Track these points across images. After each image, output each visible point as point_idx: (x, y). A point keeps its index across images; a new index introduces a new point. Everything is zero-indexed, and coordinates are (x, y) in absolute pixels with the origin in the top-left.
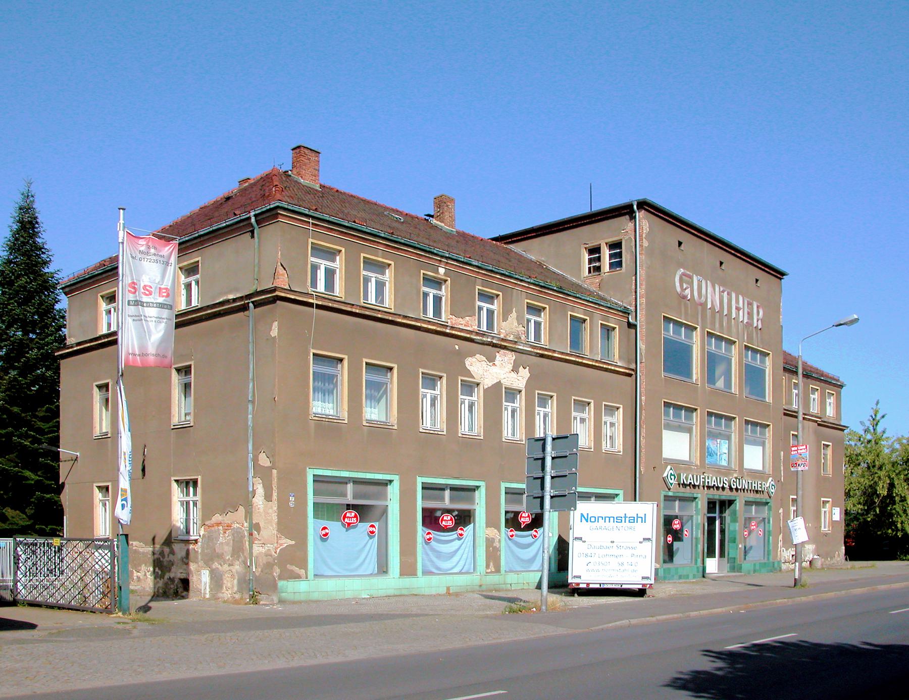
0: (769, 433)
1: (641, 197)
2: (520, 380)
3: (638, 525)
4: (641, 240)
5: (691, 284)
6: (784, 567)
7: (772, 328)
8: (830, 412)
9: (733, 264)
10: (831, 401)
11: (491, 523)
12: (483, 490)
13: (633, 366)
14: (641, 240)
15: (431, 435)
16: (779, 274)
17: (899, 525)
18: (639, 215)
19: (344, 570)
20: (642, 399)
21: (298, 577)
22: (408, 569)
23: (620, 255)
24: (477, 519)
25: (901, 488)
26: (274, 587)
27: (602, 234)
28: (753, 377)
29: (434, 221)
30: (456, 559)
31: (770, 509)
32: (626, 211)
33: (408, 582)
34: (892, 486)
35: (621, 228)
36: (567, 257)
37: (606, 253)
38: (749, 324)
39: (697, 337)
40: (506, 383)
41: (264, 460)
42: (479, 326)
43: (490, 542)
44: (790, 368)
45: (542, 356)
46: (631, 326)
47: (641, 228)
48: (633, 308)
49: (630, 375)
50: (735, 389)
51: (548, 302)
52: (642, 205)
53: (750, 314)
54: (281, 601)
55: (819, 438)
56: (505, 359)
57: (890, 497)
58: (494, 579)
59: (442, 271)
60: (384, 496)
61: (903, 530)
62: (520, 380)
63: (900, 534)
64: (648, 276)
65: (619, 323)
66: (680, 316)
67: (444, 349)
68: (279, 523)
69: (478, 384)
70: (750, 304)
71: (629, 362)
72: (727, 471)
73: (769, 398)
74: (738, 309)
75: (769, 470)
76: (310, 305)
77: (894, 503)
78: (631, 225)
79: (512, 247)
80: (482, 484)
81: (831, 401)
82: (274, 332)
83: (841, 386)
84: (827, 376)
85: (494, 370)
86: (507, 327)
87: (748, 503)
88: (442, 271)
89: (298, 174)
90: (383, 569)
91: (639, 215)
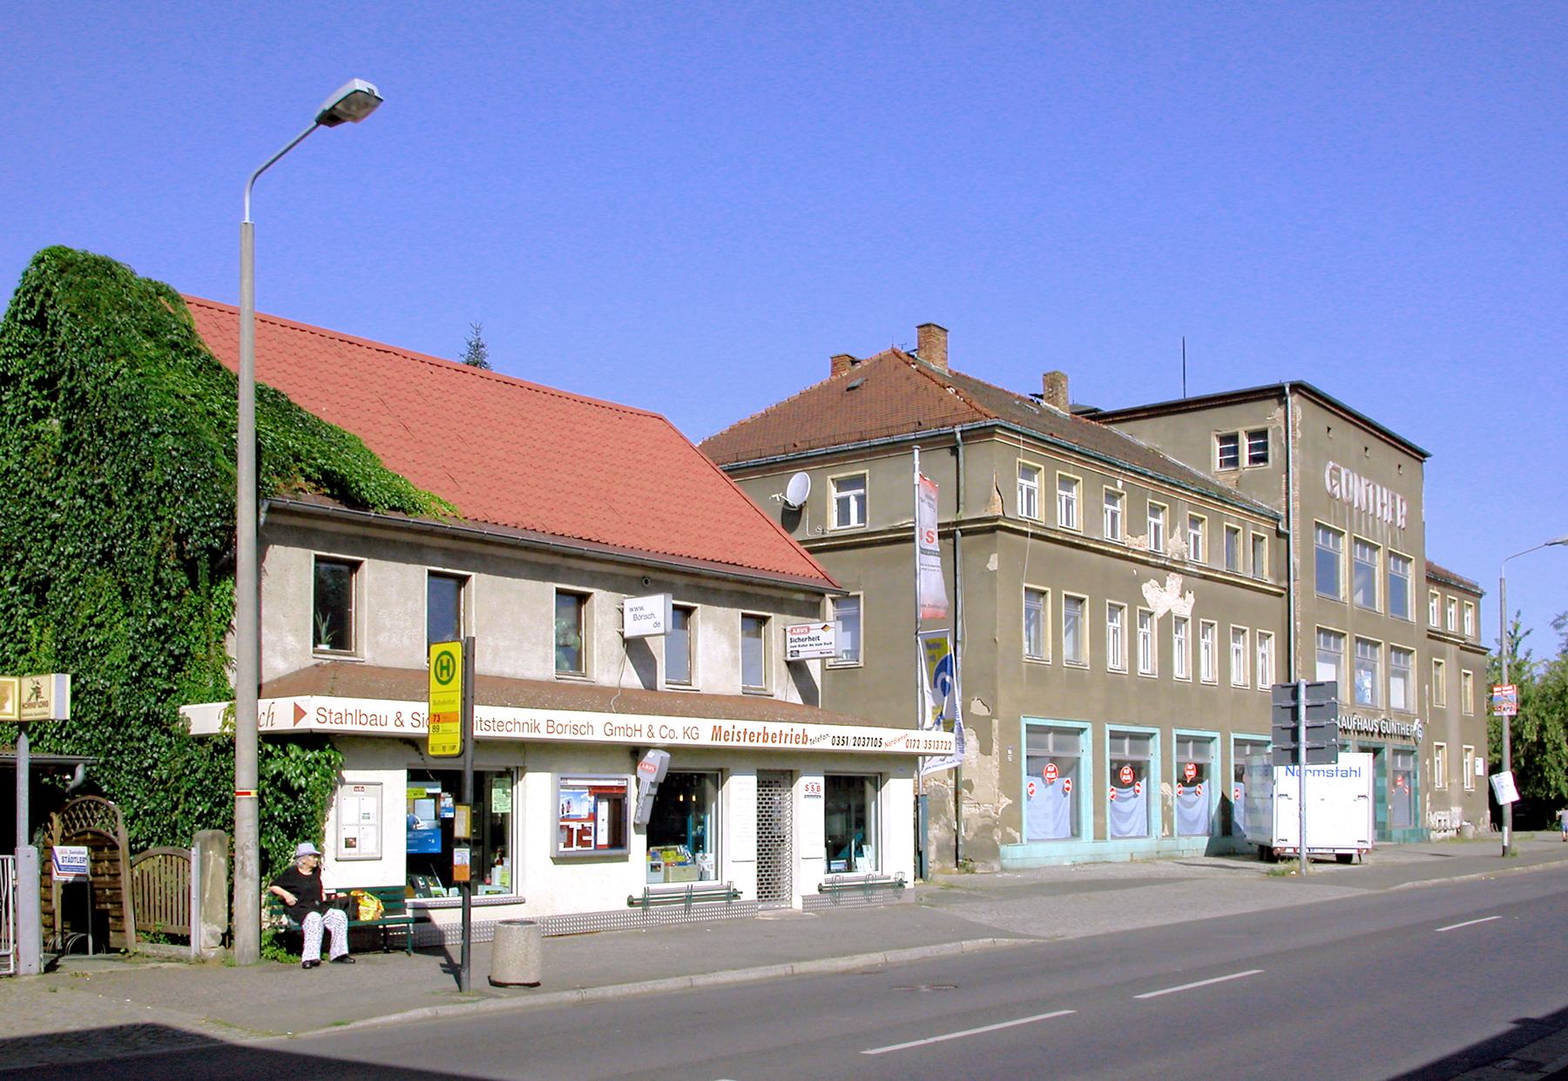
0: (1413, 661)
1: (1296, 379)
2: (1184, 607)
3: (1352, 779)
4: (1294, 430)
5: (1339, 479)
6: (1433, 835)
7: (1415, 530)
8: (1469, 630)
9: (1379, 448)
10: (1469, 614)
11: (1166, 778)
12: (1158, 737)
13: (1284, 584)
14: (1294, 430)
15: (1181, 682)
16: (1420, 455)
17: (1553, 783)
18: (1292, 400)
19: (1047, 836)
20: (1297, 625)
21: (1014, 841)
22: (1100, 835)
23: (1265, 446)
24: (1152, 773)
25: (1555, 732)
26: (994, 852)
27: (1241, 421)
28: (1396, 586)
29: (1044, 403)
30: (1132, 819)
31: (1416, 760)
32: (1275, 393)
33: (1100, 845)
34: (1542, 728)
35: (1270, 415)
36: (1196, 447)
37: (1245, 443)
38: (1393, 523)
39: (1344, 543)
40: (1175, 612)
41: (978, 708)
42: (1157, 546)
43: (1164, 799)
44: (1437, 578)
45: (1205, 577)
46: (1279, 533)
47: (1294, 416)
48: (1283, 513)
49: (1280, 595)
50: (1379, 606)
51: (1206, 511)
52: (1297, 387)
53: (1394, 511)
54: (1003, 869)
55: (1462, 664)
56: (1174, 581)
57: (1541, 744)
58: (1168, 843)
59: (1120, 484)
60: (1076, 747)
61: (1557, 789)
62: (1184, 607)
63: (1552, 795)
64: (1302, 473)
65: (1268, 531)
66: (1332, 519)
67: (1118, 572)
68: (1000, 780)
69: (1151, 614)
70: (1394, 498)
71: (1279, 579)
72: (1372, 712)
73: (1412, 616)
74: (1382, 505)
75: (1413, 708)
76: (1025, 534)
77: (1545, 752)
78: (1280, 411)
79: (1114, 428)
80: (1157, 731)
81: (1469, 614)
82: (993, 564)
83: (1480, 595)
84: (1461, 582)
85: (1165, 596)
86: (1174, 546)
87: (1396, 752)
88: (1120, 484)
89: (929, 358)
90: (1076, 832)
91: (1292, 400)
